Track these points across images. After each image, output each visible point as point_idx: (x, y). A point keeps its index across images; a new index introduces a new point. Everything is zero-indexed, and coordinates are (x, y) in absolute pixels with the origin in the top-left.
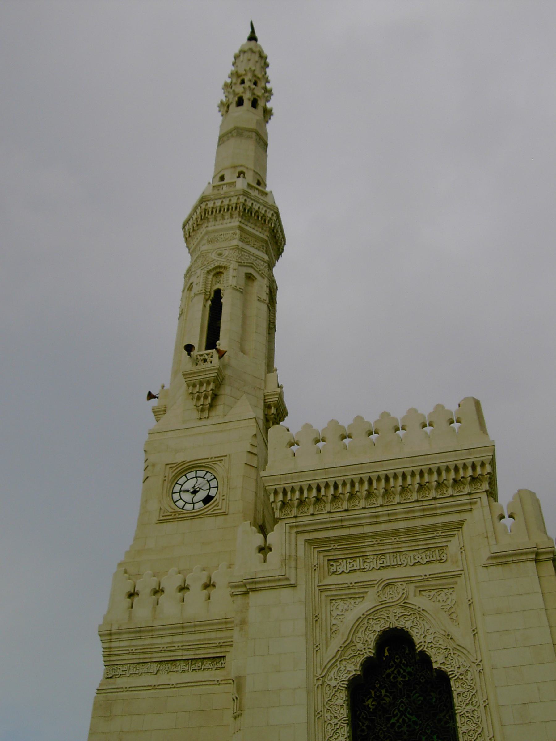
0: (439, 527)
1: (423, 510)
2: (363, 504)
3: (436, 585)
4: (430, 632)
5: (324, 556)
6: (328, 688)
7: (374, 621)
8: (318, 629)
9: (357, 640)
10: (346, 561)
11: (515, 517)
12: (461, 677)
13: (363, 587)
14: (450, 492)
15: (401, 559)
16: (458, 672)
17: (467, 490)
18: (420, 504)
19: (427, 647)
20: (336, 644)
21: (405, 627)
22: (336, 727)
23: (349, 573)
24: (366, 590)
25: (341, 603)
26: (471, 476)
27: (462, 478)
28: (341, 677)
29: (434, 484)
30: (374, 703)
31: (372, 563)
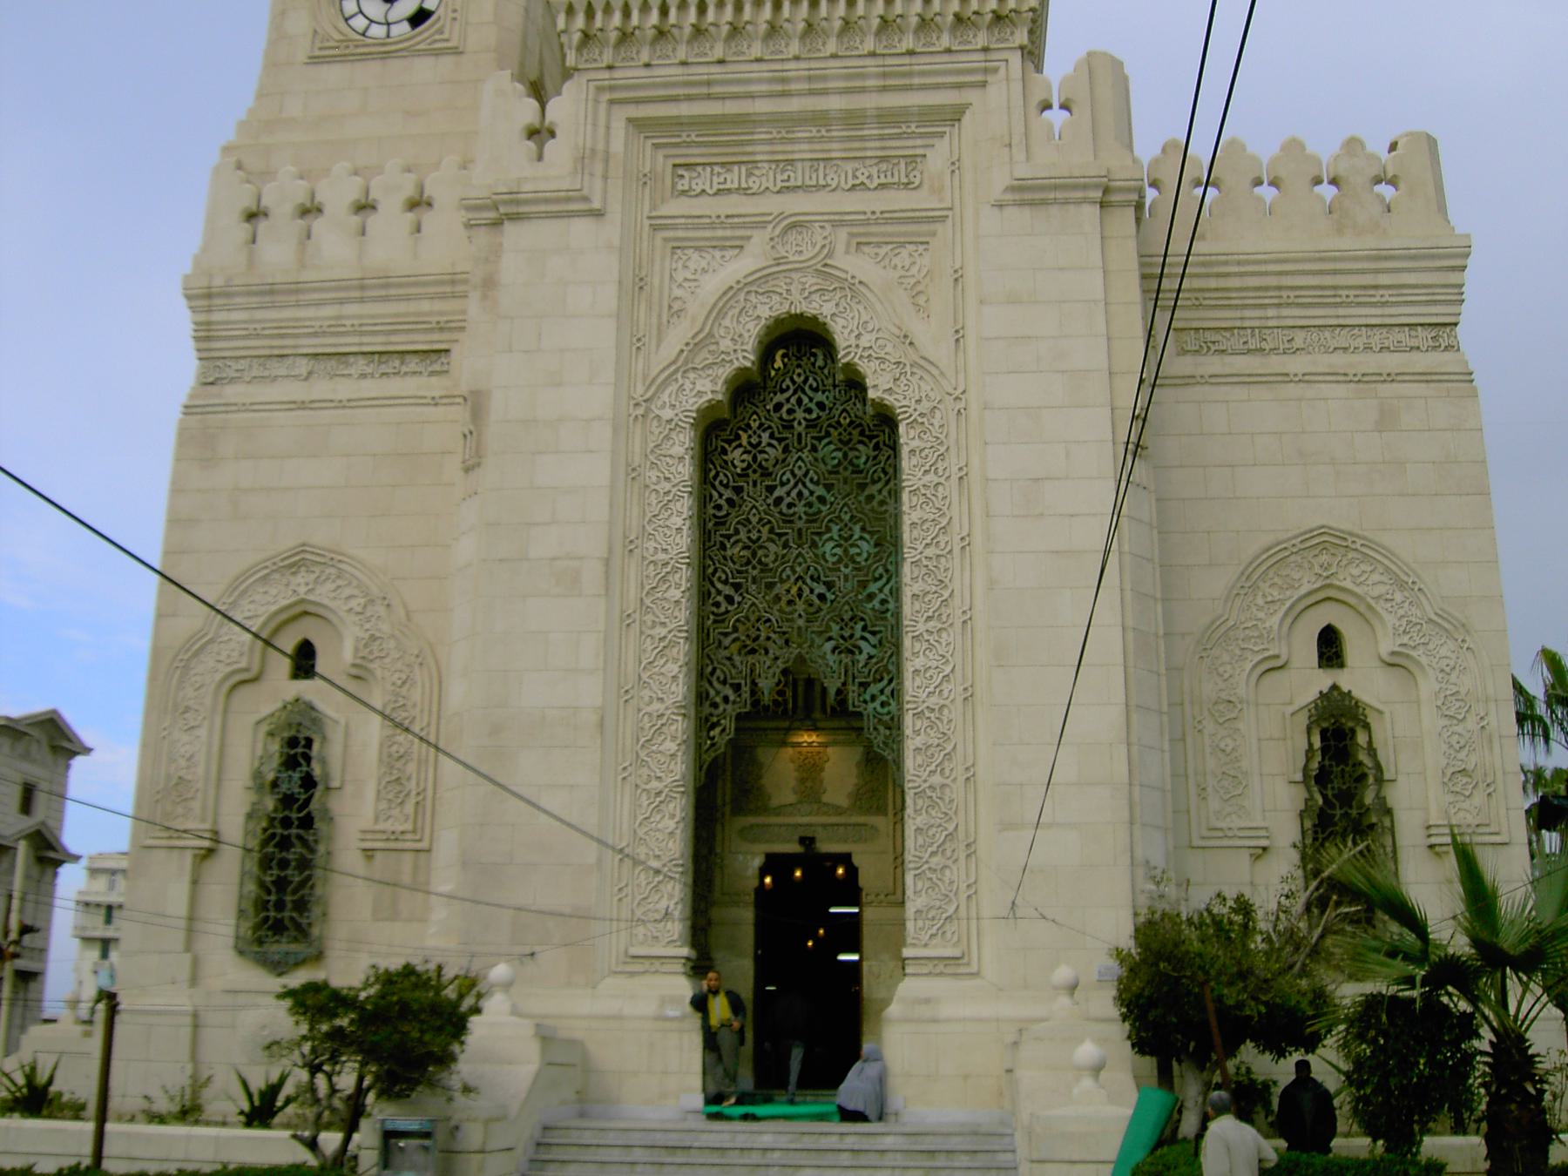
1: (884, 75)
2: (757, 50)
3: (891, 235)
4: (870, 327)
5: (666, 157)
6: (655, 423)
8: (643, 306)
9: (722, 332)
11: (1075, 110)
12: (920, 420)
13: (743, 226)
14: (946, 41)
15: (825, 175)
17: (981, 40)
18: (880, 61)
19: (861, 356)
20: (677, 337)
22: (662, 644)
23: (715, 194)
24: (748, 233)
25: (695, 256)
26: (994, 12)
27: (976, 13)
29: (914, 20)
31: (765, 178)
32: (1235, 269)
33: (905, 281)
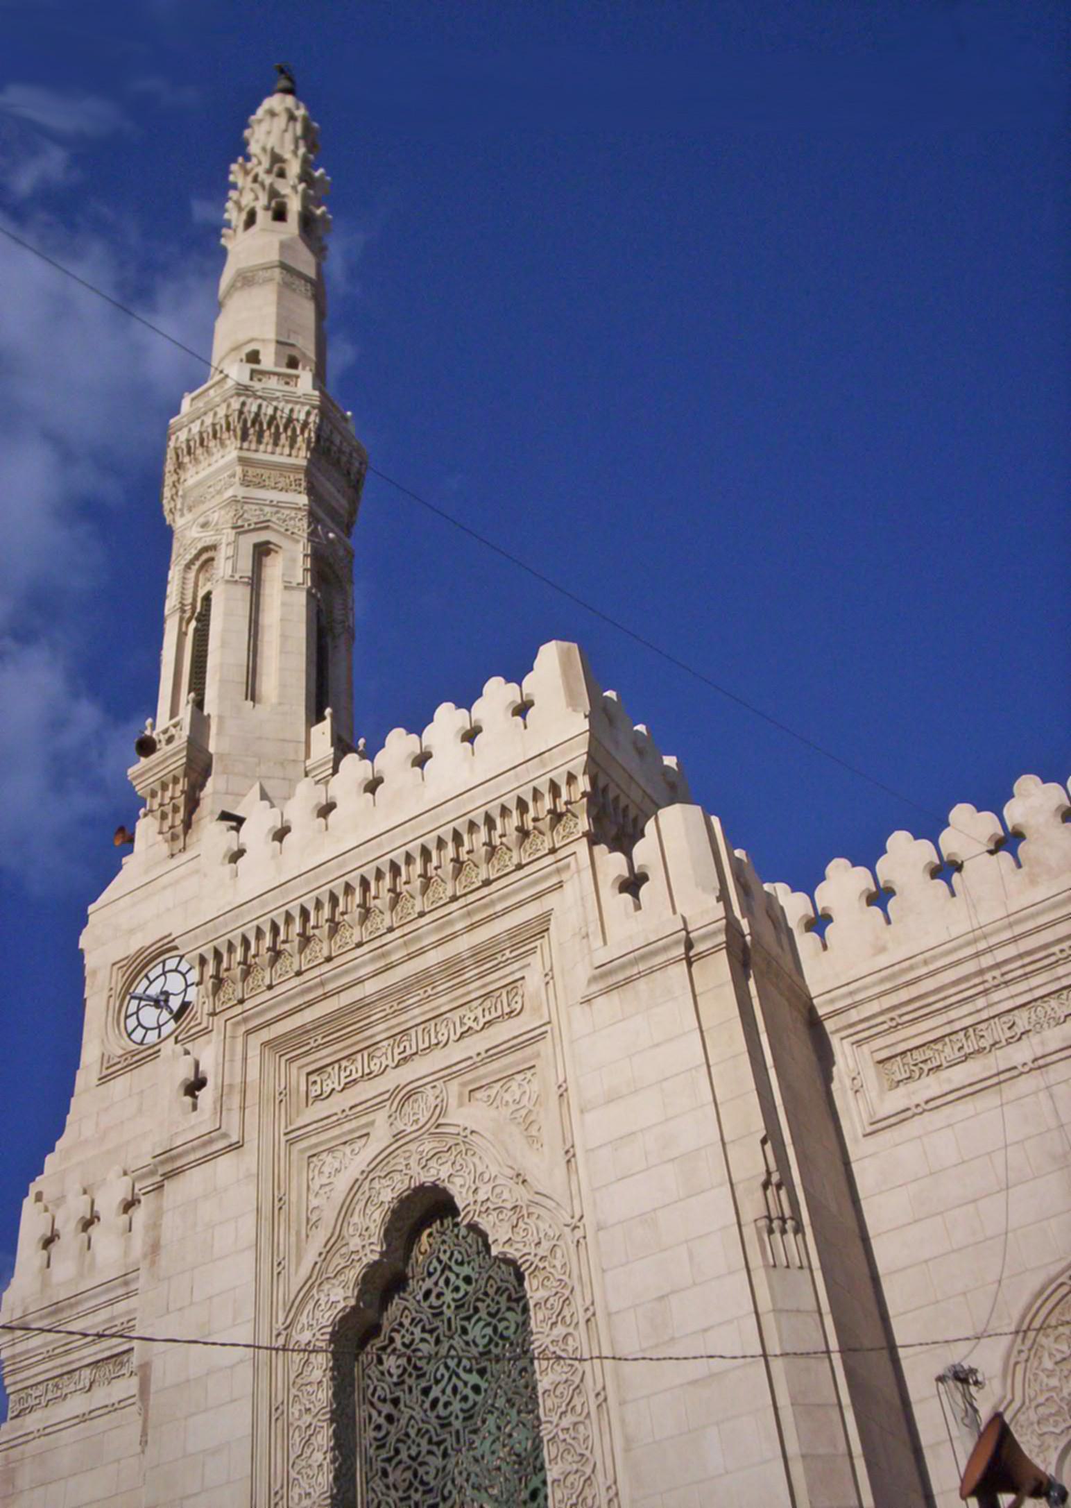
0: (504, 941)
1: (469, 914)
4: (486, 1177)
7: (383, 1181)
10: (340, 1067)
15: (437, 1033)
16: (536, 1255)
18: (462, 902)
19: (480, 1212)
21: (439, 1179)
28: (320, 1321)
30: (399, 1362)
32: (924, 970)
33: (517, 1115)
